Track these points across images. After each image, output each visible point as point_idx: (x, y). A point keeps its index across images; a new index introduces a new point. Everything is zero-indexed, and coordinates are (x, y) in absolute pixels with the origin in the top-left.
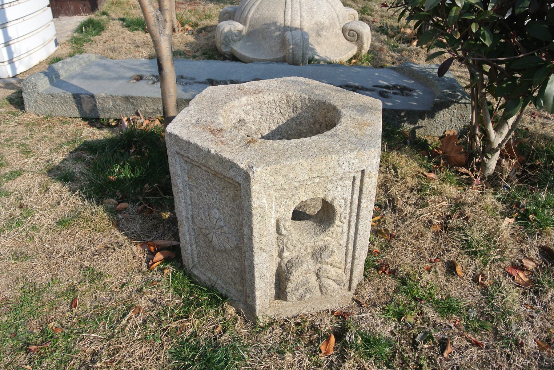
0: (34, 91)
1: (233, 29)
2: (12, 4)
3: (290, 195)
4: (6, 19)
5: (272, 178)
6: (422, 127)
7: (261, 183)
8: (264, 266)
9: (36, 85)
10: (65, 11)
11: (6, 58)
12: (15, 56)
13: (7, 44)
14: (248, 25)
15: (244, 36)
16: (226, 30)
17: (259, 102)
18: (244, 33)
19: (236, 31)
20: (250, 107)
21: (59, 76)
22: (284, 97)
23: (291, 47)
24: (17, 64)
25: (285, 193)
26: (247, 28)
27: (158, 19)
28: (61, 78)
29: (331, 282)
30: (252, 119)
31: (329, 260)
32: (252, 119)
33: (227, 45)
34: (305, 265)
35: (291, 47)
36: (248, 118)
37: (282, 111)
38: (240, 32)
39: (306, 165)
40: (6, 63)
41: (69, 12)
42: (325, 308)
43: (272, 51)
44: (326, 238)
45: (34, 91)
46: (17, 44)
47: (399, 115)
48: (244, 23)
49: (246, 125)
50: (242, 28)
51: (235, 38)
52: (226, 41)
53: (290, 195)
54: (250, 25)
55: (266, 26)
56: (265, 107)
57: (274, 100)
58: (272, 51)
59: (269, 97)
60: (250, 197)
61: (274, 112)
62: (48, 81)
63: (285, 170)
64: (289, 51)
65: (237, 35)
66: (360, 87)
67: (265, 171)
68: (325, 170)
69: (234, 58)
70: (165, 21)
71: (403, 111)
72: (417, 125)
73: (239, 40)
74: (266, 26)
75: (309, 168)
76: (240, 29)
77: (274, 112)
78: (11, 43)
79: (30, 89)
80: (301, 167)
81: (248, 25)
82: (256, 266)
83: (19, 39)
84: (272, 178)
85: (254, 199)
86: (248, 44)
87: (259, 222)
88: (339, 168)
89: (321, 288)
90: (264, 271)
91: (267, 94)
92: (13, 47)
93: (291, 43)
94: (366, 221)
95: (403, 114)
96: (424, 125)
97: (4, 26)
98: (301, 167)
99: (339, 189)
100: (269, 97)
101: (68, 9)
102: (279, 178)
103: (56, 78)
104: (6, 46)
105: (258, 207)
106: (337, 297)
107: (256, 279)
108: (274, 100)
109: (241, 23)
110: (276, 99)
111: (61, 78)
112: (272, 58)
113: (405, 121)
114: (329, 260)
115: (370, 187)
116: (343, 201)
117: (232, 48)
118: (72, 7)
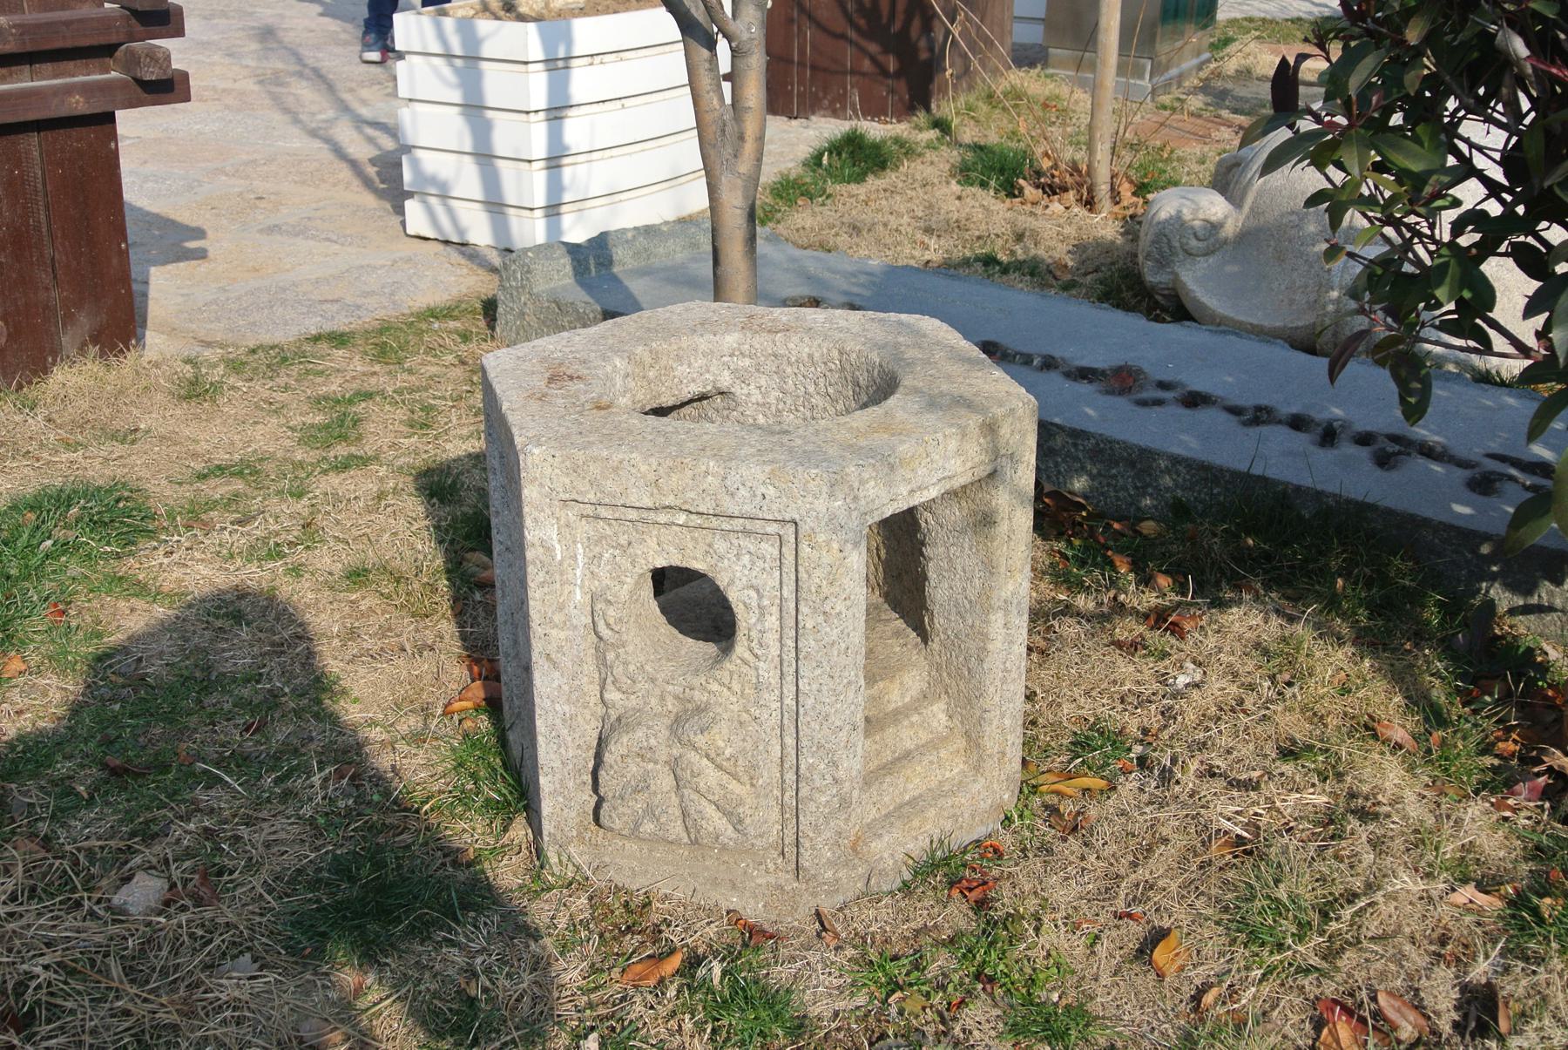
0: (523, 287)
1: (1187, 215)
2: (597, 59)
3: (623, 540)
4: (568, 97)
5: (567, 481)
6: (1551, 609)
7: (541, 485)
8: (558, 707)
9: (528, 272)
10: (832, 103)
11: (540, 199)
12: (567, 197)
13: (553, 163)
14: (1246, 208)
15: (1225, 241)
16: (1163, 215)
17: (775, 356)
18: (1230, 230)
19: (1197, 223)
20: (747, 362)
21: (611, 262)
22: (835, 354)
23: (1335, 294)
24: (567, 220)
25: (609, 532)
26: (1242, 218)
27: (723, 131)
28: (616, 270)
29: (710, 810)
30: (757, 397)
31: (700, 740)
32: (757, 397)
33: (1163, 262)
34: (640, 734)
35: (1335, 294)
36: (745, 391)
37: (831, 390)
38: (1214, 227)
39: (644, 468)
40: (539, 213)
41: (844, 108)
42: (724, 906)
43: (1292, 302)
44: (715, 687)
45: (523, 287)
46: (581, 169)
47: (1475, 551)
48: (1236, 200)
49: (741, 409)
50: (1220, 215)
51: (1194, 243)
52: (1161, 252)
53: (623, 540)
54: (1252, 209)
55: (1294, 217)
56: (789, 370)
57: (811, 356)
58: (1292, 302)
59: (799, 347)
60: (520, 514)
61: (811, 389)
62: (569, 269)
63: (594, 469)
64: (1324, 307)
65: (1200, 234)
66: (1439, 449)
67: (550, 459)
68: (692, 495)
69: (1176, 309)
70: (741, 138)
71: (1486, 537)
72: (1534, 600)
73: (1208, 253)
74: (1294, 217)
75: (652, 477)
76: (1213, 219)
77: (811, 389)
78: (566, 161)
79: (515, 279)
80: (634, 471)
81: (1246, 208)
82: (537, 700)
83: (595, 155)
84: (567, 481)
85: (528, 522)
86: (1229, 268)
87: (542, 585)
88: (728, 498)
89: (685, 814)
90: (558, 721)
91: (795, 339)
92: (567, 173)
93: (1336, 280)
94: (818, 671)
95: (1485, 549)
96: (1558, 602)
97: (558, 114)
98: (634, 471)
99: (746, 559)
100: (799, 347)
101: (843, 98)
102: (583, 486)
103: (599, 265)
104: (548, 168)
105: (538, 544)
106: (759, 881)
107: (540, 739)
108: (811, 356)
109: (1229, 199)
110: (817, 355)
111: (616, 270)
112: (1278, 324)
113: (1493, 578)
114: (700, 740)
115: (817, 573)
116: (753, 594)
117: (1176, 275)
118: (856, 92)
